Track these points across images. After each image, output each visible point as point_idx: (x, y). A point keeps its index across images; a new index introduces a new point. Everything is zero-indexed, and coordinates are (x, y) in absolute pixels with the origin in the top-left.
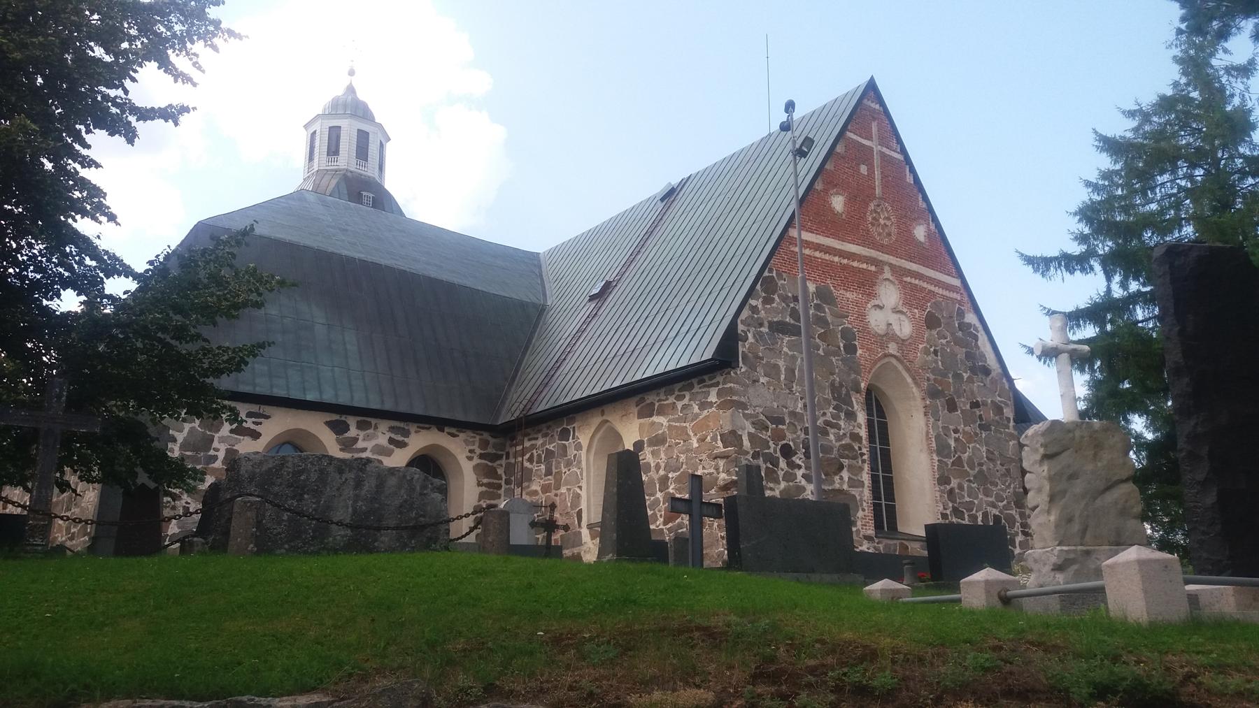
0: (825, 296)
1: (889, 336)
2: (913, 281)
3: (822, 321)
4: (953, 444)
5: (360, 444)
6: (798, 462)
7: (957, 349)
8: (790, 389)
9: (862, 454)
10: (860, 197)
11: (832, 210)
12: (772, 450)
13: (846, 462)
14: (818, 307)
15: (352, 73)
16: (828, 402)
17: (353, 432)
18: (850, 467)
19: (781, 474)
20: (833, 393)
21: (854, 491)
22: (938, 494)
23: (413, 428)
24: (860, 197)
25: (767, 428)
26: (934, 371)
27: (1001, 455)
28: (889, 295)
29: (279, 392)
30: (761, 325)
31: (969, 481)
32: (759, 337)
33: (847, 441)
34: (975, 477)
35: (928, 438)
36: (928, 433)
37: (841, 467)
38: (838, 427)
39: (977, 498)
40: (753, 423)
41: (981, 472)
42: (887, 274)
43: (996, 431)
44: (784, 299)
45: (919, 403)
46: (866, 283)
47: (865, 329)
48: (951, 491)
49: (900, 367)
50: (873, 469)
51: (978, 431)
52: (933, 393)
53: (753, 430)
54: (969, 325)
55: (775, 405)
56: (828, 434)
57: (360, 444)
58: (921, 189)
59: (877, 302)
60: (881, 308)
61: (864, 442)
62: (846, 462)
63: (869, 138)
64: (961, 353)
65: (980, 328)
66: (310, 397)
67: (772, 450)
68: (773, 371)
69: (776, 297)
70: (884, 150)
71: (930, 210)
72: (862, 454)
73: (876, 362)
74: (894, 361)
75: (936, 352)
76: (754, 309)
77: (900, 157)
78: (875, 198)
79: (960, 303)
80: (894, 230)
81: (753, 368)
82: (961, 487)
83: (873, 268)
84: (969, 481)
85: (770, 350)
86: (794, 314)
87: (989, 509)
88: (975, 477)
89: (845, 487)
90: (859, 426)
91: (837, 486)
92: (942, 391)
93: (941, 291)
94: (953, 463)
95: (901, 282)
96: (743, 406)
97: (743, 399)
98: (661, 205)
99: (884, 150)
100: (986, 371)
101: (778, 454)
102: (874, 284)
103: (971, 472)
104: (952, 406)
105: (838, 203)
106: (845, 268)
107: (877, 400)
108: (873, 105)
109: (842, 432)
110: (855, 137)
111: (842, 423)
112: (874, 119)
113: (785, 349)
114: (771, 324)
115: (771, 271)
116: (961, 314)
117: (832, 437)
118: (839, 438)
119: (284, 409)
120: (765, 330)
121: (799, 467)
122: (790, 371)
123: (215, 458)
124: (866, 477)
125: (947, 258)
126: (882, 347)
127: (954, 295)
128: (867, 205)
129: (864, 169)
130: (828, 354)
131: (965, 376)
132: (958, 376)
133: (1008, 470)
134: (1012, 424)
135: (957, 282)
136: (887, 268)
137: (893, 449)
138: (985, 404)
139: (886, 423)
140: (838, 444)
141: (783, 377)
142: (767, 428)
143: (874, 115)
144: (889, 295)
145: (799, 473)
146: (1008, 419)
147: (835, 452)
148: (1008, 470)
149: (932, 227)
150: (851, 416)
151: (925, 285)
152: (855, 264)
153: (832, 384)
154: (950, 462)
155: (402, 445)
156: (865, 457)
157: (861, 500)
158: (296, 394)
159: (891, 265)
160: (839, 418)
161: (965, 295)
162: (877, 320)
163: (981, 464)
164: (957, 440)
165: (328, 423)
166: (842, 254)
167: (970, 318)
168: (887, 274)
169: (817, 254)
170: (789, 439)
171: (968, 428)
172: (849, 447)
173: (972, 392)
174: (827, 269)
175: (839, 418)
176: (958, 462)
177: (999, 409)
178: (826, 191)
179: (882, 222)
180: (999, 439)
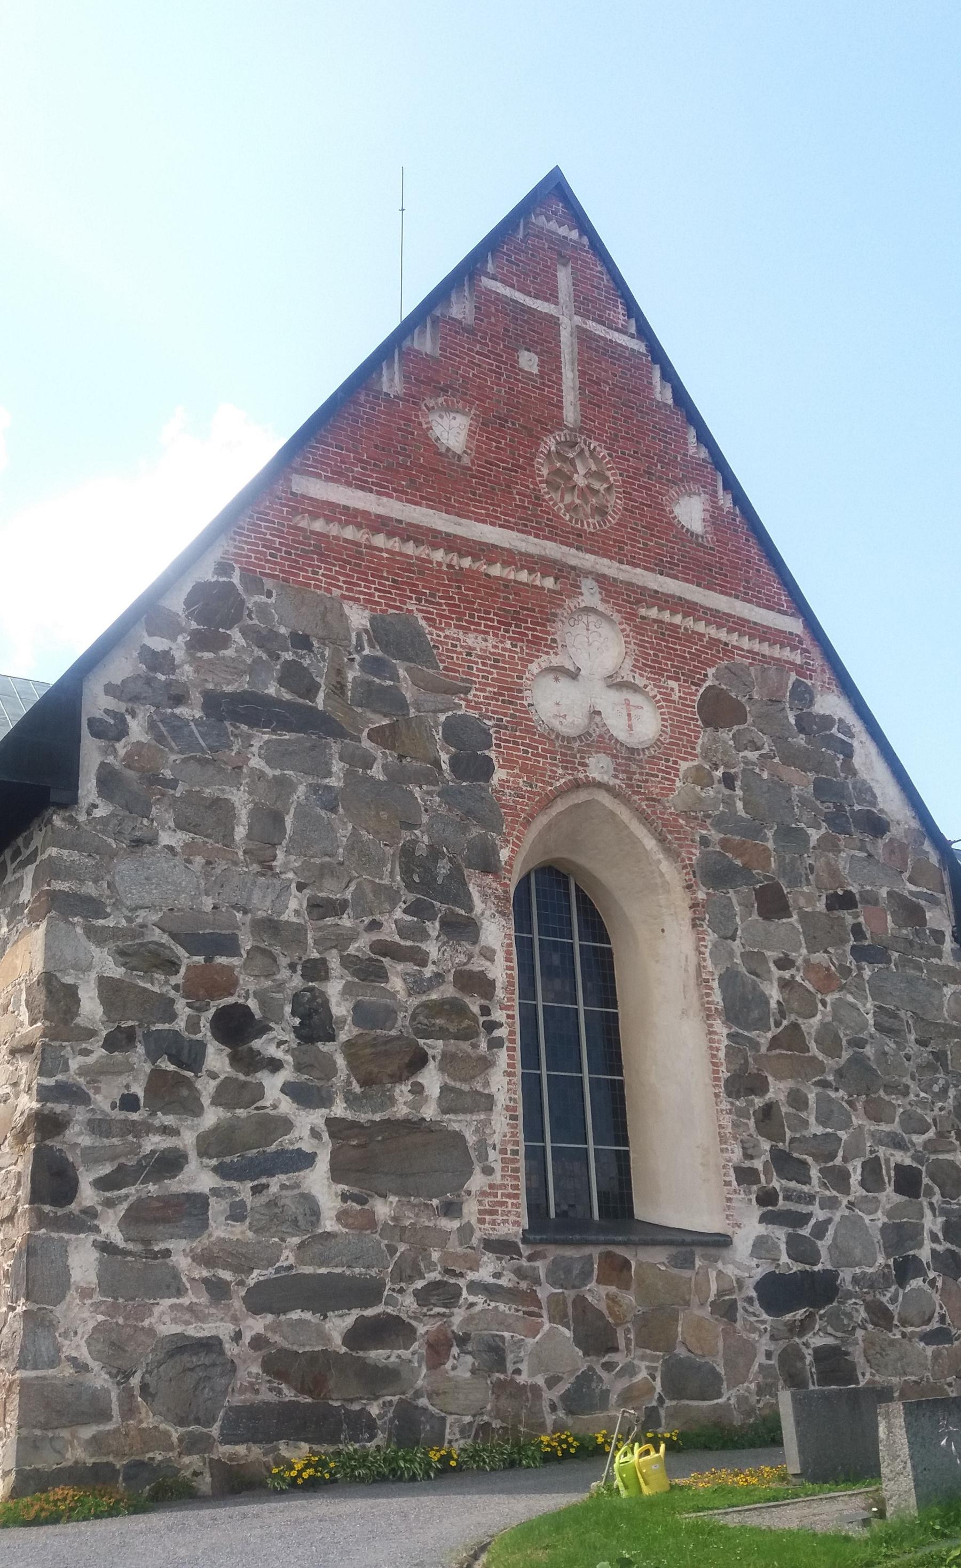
0: (396, 639)
1: (596, 739)
2: (666, 616)
3: (392, 701)
4: (774, 994)
6: (273, 1051)
7: (791, 774)
8: (267, 867)
9: (492, 1026)
10: (516, 421)
11: (431, 445)
12: (180, 1024)
13: (434, 1047)
14: (373, 665)
16: (393, 897)
18: (448, 1062)
19: (207, 1088)
20: (407, 873)
21: (460, 1124)
22: (727, 1120)
24: (516, 421)
25: (171, 966)
26: (719, 823)
27: (918, 1018)
28: (598, 645)
30: (179, 699)
31: (824, 1084)
33: (448, 991)
34: (839, 1073)
35: (703, 983)
36: (700, 968)
37: (419, 1061)
38: (421, 959)
39: (847, 1125)
40: (122, 953)
41: (858, 1061)
42: (590, 595)
43: (904, 963)
45: (679, 900)
46: (529, 617)
47: (522, 723)
48: (768, 1111)
49: (624, 814)
50: (530, 1057)
51: (850, 961)
52: (717, 874)
53: (117, 972)
54: (827, 721)
55: (208, 903)
56: (382, 975)
58: (693, 417)
59: (556, 661)
60: (574, 675)
61: (500, 993)
62: (434, 1047)
63: (551, 296)
64: (801, 784)
65: (852, 719)
67: (180, 1024)
68: (207, 818)
69: (236, 634)
70: (591, 325)
71: (718, 462)
72: (492, 1026)
73: (548, 802)
74: (605, 799)
75: (728, 781)
77: (638, 346)
78: (560, 424)
79: (800, 670)
80: (615, 502)
81: (137, 806)
82: (798, 1100)
83: (549, 583)
84: (824, 1084)
85: (203, 762)
86: (295, 677)
87: (882, 1152)
88: (839, 1073)
89: (430, 1112)
90: (488, 954)
91: (401, 1110)
92: (746, 868)
93: (745, 643)
94: (775, 1043)
95: (630, 617)
96: (91, 907)
97: (89, 889)
99: (591, 325)
100: (876, 825)
101: (205, 1032)
102: (551, 618)
103: (829, 1062)
104: (772, 904)
105: (452, 431)
106: (460, 576)
107: (584, 900)
108: (563, 231)
109: (428, 971)
111: (432, 949)
112: (564, 259)
113: (255, 762)
116: (803, 695)
117: (397, 984)
118: (417, 986)
120: (191, 712)
121: (275, 1065)
122: (268, 822)
124: (503, 1083)
125: (766, 569)
126: (568, 764)
127: (787, 654)
128: (536, 440)
129: (529, 361)
130: (397, 777)
131: (814, 835)
132: (791, 836)
133: (939, 1056)
134: (948, 945)
135: (794, 625)
136: (588, 585)
137: (626, 1009)
138: (871, 899)
139: (609, 952)
140: (414, 1002)
141: (240, 832)
142: (171, 966)
143: (561, 252)
144: (598, 645)
145: (272, 1085)
146: (938, 936)
147: (403, 1020)
148: (939, 1056)
149: (725, 501)
150: (462, 929)
151: (701, 627)
152: (496, 570)
153: (407, 852)
154: (764, 1039)
156: (502, 1032)
157: (482, 1145)
159: (602, 580)
160: (425, 936)
161: (816, 652)
162: (556, 704)
163: (858, 1043)
164: (785, 985)
166: (452, 543)
167: (831, 704)
168: (590, 595)
169: (380, 540)
170: (248, 992)
171: (819, 957)
172: (455, 1009)
173: (834, 873)
174: (407, 577)
175: (425, 936)
176: (792, 1038)
177: (911, 913)
179: (579, 480)
180: (910, 981)
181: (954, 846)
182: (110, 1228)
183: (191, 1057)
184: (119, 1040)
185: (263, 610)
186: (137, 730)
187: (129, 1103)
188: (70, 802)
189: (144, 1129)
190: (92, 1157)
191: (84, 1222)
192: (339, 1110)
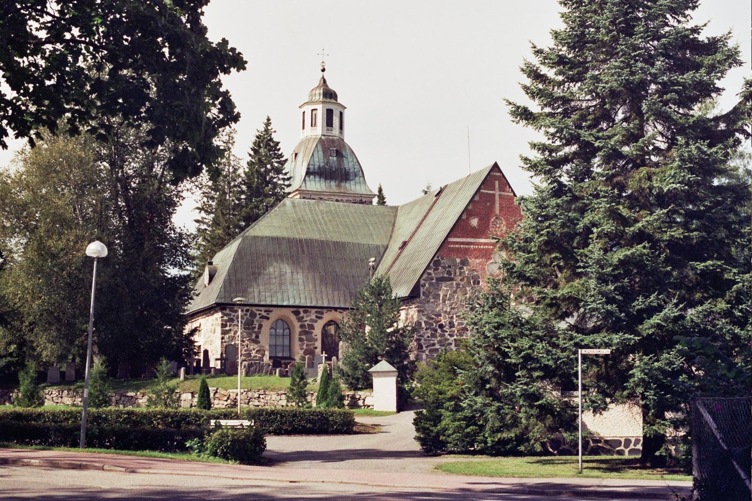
5: (305, 319)
15: (323, 70)
17: (302, 314)
19: (438, 335)
23: (325, 311)
29: (274, 303)
30: (433, 279)
32: (431, 284)
44: (444, 268)
57: (305, 319)
66: (285, 303)
76: (430, 274)
81: (427, 296)
98: (435, 198)
110: (485, 191)
114: (437, 279)
115: (438, 257)
119: (180, 490)
120: (434, 281)
123: (255, 328)
145: (446, 334)
155: (320, 318)
158: (280, 303)
165: (292, 312)
169: (462, 246)
170: (443, 322)
178: (468, 219)
181: (395, 370)
182: (427, 352)
183: (436, 331)
184: (427, 329)
185: (444, 263)
186: (427, 285)
187: (428, 337)
188: (419, 297)
189: (430, 340)
190: (424, 344)
191: (424, 352)
192: (455, 337)
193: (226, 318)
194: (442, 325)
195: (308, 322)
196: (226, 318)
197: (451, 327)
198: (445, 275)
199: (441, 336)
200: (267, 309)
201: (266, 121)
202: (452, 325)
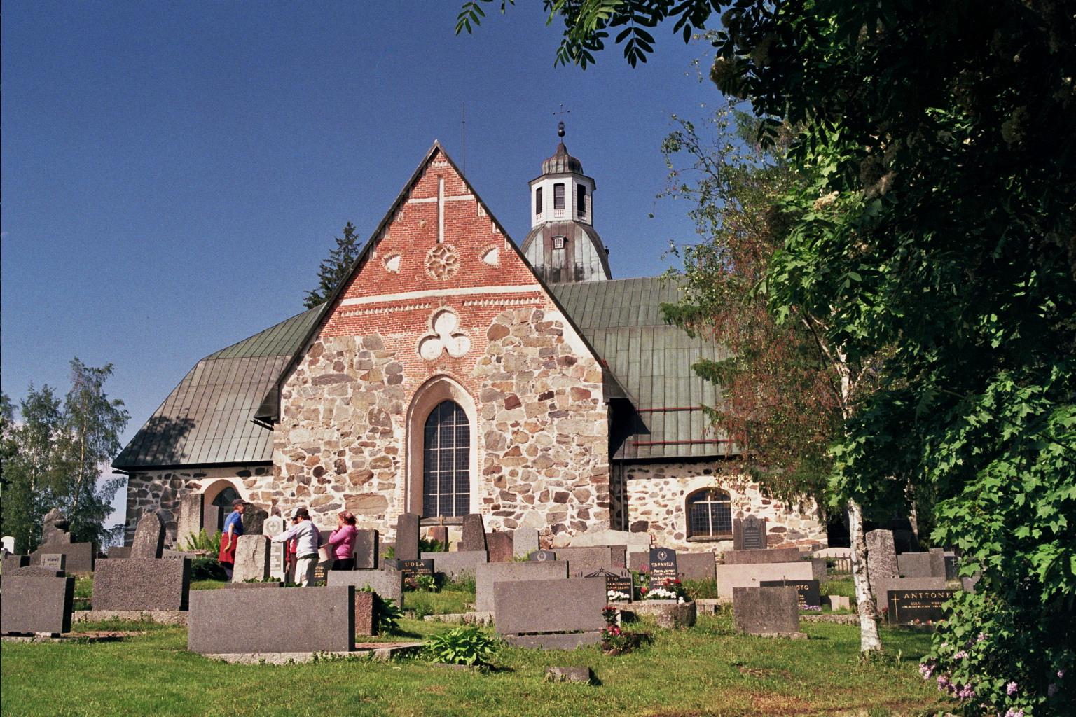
44: (329, 358)
183: (307, 482)
184: (291, 479)
186: (294, 395)
187: (293, 495)
193: (135, 490)
194: (321, 468)
195: (263, 489)
196: (135, 490)
197: (338, 473)
198: (332, 372)
199: (320, 490)
200: (198, 471)
201: (343, 237)
202: (341, 469)
